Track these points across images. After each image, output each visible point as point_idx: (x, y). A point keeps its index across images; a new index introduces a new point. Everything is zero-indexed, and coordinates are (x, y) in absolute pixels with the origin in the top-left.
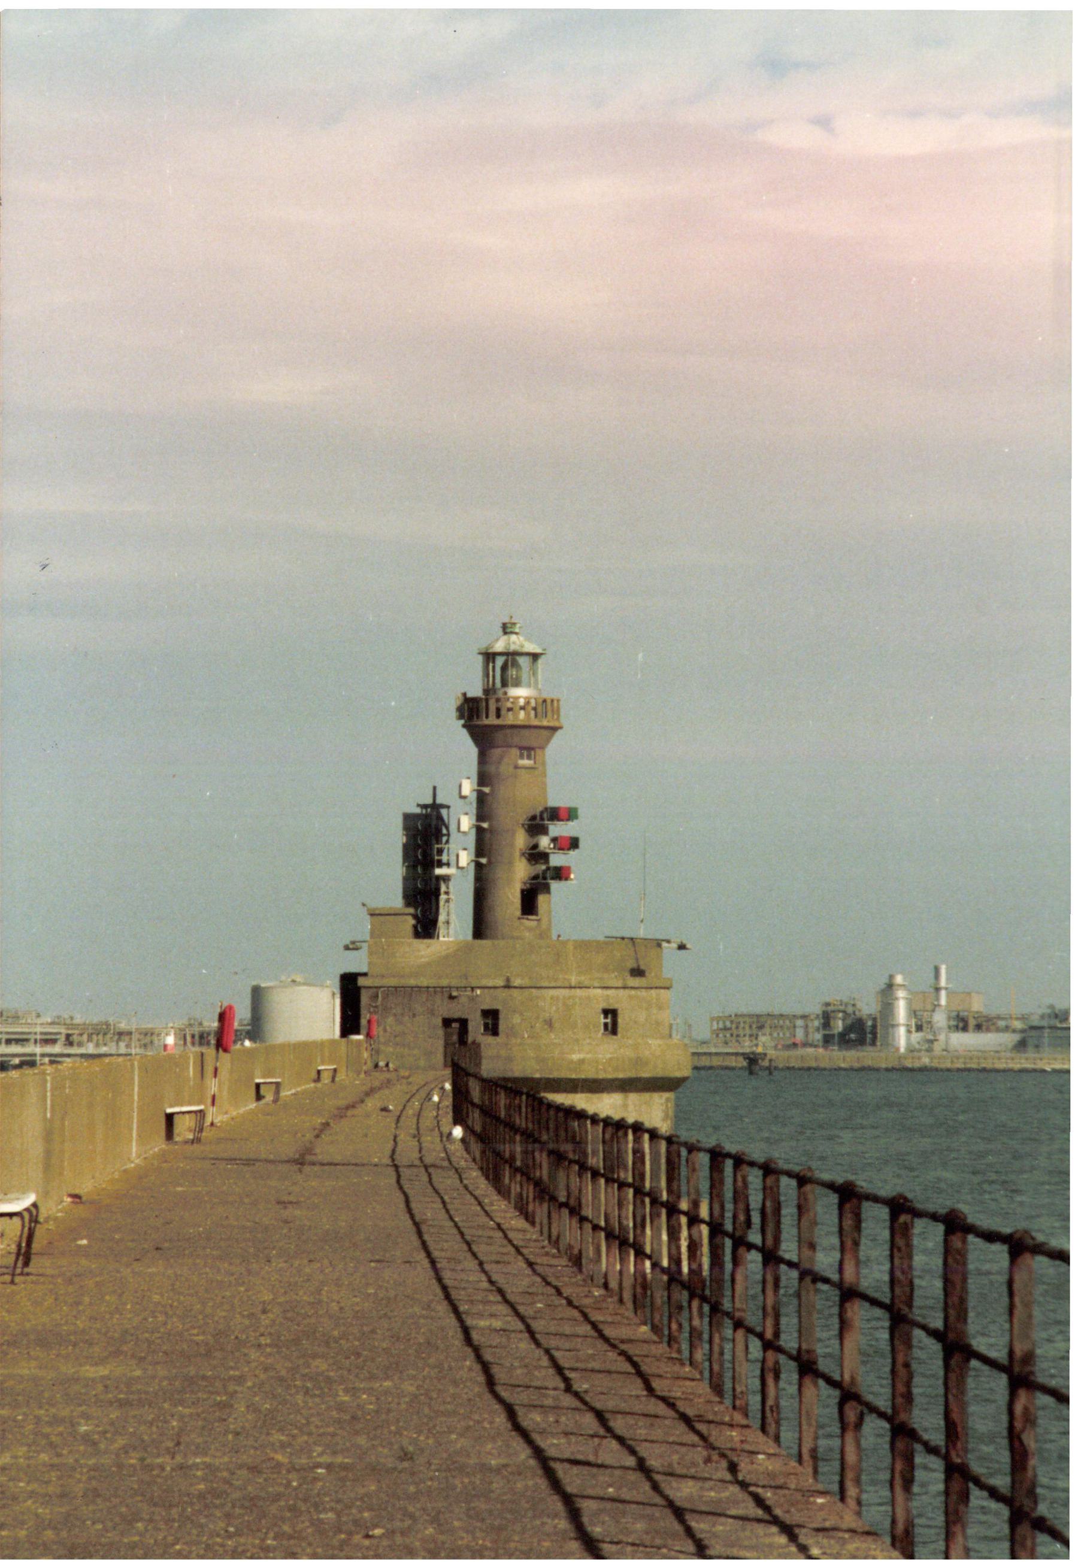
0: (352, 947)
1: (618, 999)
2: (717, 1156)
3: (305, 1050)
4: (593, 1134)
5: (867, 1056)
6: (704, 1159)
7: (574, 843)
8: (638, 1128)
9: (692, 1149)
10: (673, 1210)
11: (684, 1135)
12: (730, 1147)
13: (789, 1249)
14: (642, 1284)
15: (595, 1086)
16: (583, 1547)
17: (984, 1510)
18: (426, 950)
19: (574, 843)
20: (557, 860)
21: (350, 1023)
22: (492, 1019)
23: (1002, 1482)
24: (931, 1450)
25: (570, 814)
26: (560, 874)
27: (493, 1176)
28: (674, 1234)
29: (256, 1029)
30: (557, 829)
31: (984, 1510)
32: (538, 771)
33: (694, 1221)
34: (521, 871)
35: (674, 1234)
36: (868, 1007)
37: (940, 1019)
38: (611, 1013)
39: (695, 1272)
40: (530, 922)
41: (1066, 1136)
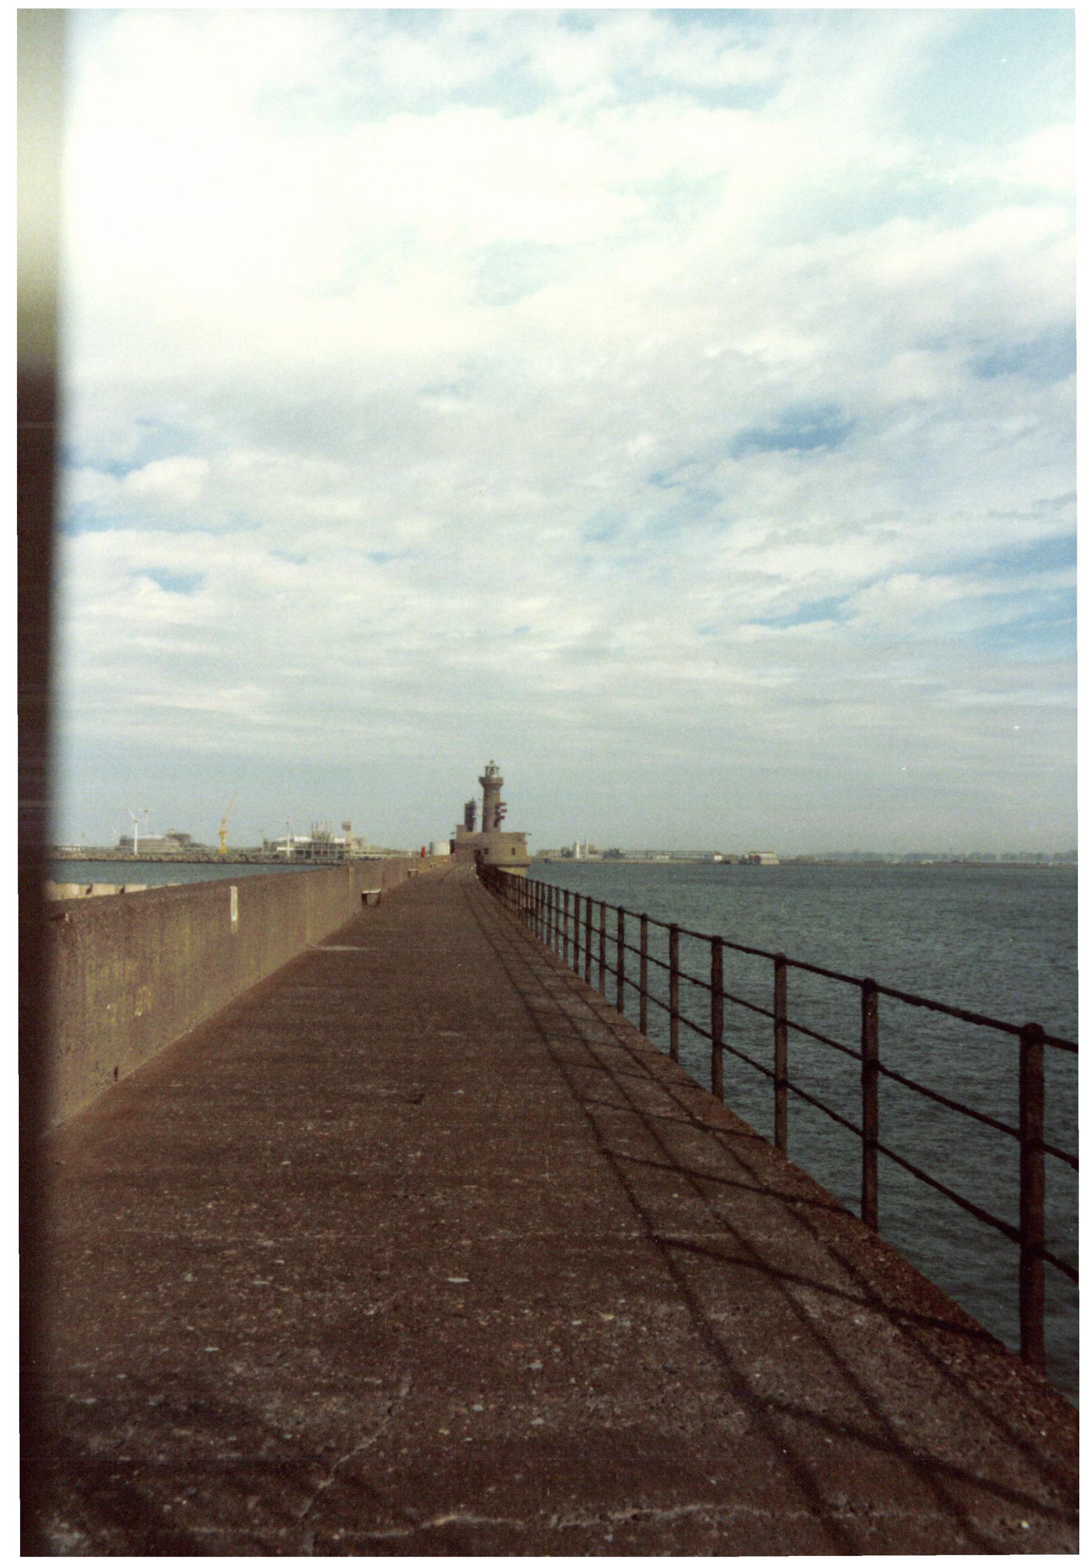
0: (453, 834)
1: (515, 846)
2: (538, 883)
3: (442, 857)
4: (509, 879)
5: (571, 859)
6: (534, 884)
7: (505, 811)
8: (519, 877)
9: (532, 881)
10: (527, 895)
11: (529, 878)
12: (541, 881)
13: (554, 904)
14: (519, 910)
15: (510, 866)
16: (56, 669)
17: (798, 1112)
18: (470, 835)
19: (505, 811)
20: (502, 814)
21: (452, 851)
22: (487, 851)
23: (615, 968)
24: (583, 950)
25: (504, 804)
26: (503, 818)
27: (486, 886)
28: (527, 900)
29: (431, 852)
30: (502, 808)
31: (798, 1112)
32: (498, 794)
33: (532, 898)
34: (494, 817)
35: (527, 900)
36: (571, 849)
37: (586, 851)
38: (513, 850)
39: (532, 910)
40: (495, 829)
41: (30, 425)
